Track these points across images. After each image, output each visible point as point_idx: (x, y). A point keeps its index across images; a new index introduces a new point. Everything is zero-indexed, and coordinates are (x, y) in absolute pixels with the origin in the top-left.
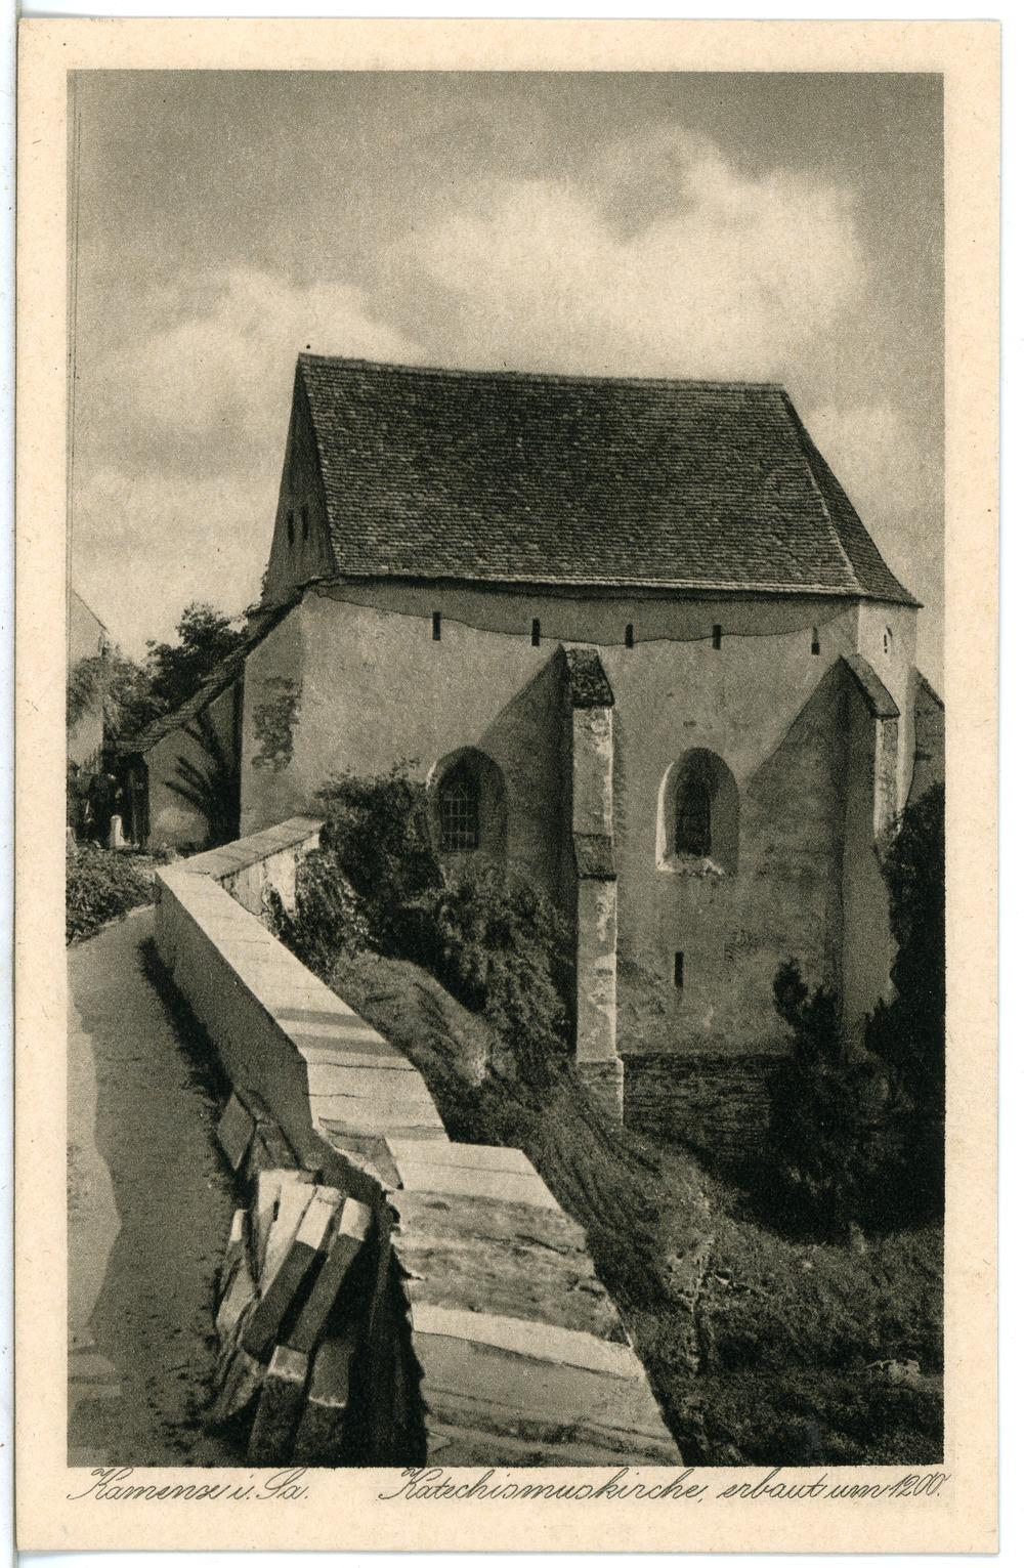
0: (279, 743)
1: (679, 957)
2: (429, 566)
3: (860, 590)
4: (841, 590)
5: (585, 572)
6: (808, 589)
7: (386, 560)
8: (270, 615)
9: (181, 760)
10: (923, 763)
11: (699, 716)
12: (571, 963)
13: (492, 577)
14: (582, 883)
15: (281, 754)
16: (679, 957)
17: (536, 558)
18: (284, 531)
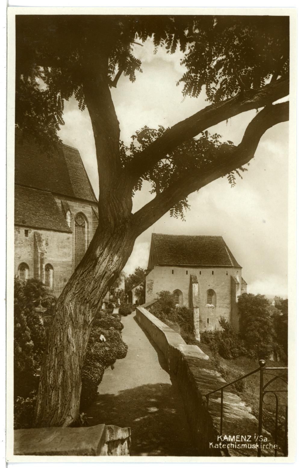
0: (151, 289)
1: (208, 319)
2: (172, 263)
3: (233, 266)
4: (231, 266)
5: (194, 264)
6: (226, 266)
7: (165, 262)
8: (149, 270)
9: (177, 85)
10: (243, 291)
11: (211, 284)
12: (130, 437)
13: (181, 265)
14: (194, 309)
15: (151, 291)
16: (208, 319)
17: (187, 262)
18: (151, 260)
